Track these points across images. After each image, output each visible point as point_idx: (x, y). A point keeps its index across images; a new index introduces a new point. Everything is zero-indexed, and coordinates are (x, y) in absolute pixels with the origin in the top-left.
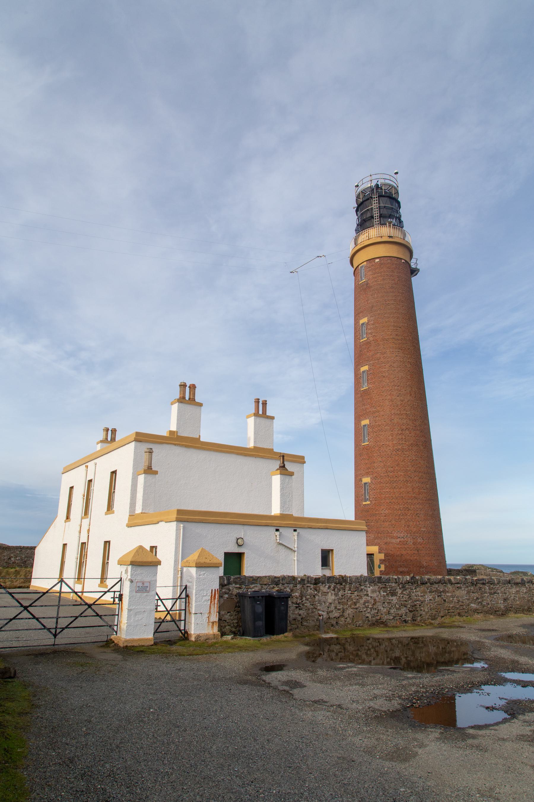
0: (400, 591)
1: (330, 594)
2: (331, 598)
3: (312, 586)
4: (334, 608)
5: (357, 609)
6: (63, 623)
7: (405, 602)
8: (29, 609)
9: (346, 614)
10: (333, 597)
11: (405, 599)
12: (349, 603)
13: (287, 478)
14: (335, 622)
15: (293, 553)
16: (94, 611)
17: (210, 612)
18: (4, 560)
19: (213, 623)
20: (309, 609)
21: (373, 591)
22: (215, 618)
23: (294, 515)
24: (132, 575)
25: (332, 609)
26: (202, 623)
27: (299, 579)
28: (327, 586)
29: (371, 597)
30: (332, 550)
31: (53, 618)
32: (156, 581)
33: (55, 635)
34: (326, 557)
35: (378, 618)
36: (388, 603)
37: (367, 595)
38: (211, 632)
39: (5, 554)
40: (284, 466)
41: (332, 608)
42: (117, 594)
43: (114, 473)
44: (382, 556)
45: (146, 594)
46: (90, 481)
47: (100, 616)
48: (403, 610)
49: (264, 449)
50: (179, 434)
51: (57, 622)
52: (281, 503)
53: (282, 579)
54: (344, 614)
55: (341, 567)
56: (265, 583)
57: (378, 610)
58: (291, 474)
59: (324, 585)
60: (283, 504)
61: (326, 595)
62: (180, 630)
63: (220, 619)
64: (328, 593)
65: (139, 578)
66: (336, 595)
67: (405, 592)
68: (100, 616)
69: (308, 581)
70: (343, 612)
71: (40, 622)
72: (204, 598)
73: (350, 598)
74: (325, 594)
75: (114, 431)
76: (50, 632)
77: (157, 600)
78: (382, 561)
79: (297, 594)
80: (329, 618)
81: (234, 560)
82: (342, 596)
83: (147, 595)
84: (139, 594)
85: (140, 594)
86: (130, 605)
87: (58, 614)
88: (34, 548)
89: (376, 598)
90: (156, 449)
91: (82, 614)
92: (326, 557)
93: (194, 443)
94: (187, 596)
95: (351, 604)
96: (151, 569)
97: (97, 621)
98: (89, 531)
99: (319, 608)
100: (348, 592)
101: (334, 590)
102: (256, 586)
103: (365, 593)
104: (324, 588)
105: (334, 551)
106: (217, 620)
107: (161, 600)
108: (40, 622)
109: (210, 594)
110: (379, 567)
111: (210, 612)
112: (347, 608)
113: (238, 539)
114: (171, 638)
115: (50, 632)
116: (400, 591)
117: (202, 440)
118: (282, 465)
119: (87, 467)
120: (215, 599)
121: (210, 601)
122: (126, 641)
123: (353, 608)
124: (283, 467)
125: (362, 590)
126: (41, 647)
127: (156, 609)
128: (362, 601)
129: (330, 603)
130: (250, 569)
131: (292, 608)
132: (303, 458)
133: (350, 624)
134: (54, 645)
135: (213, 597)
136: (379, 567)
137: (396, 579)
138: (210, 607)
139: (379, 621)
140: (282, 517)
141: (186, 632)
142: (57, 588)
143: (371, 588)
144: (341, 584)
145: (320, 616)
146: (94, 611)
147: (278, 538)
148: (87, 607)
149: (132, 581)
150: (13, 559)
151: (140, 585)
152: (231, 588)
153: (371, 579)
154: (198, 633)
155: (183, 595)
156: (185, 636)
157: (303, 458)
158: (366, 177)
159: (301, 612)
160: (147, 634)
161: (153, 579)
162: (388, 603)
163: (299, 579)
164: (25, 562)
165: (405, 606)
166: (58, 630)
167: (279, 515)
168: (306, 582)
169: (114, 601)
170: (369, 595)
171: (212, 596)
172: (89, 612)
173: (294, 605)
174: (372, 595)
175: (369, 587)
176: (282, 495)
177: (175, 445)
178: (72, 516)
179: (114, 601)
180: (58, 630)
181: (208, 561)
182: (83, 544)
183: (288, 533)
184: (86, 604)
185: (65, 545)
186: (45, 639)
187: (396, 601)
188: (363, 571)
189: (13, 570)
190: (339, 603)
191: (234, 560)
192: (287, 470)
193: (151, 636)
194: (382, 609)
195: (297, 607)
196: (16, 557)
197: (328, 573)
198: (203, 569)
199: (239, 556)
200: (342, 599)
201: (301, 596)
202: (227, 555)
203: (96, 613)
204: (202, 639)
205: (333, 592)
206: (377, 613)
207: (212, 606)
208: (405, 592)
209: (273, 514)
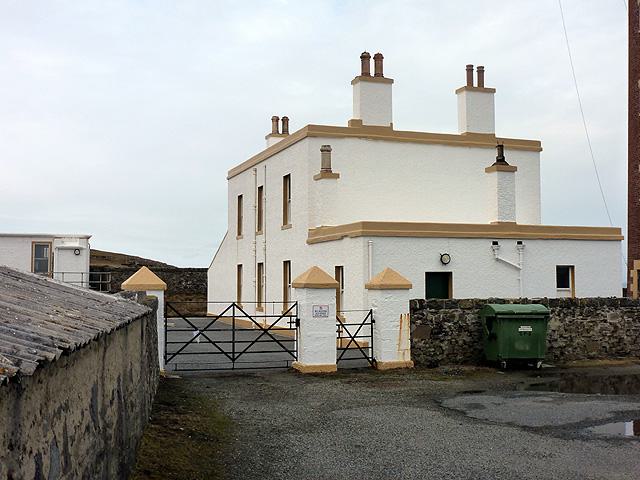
6: (239, 347)
13: (508, 175)
22: (407, 345)
26: (393, 348)
33: (233, 360)
34: (564, 275)
37: (605, 321)
42: (294, 319)
43: (287, 178)
46: (261, 188)
55: (585, 288)
58: (513, 170)
62: (368, 358)
63: (412, 347)
66: (561, 321)
75: (285, 120)
81: (438, 283)
89: (619, 325)
90: (333, 144)
92: (564, 275)
93: (385, 134)
97: (275, 346)
101: (559, 315)
107: (343, 326)
114: (356, 365)
124: (501, 160)
128: (597, 329)
129: (554, 331)
130: (459, 292)
134: (233, 369)
140: (501, 226)
141: (374, 360)
142: (229, 313)
153: (623, 302)
155: (369, 321)
166: (236, 355)
177: (360, 137)
182: (260, 265)
184: (262, 329)
185: (240, 266)
186: (224, 363)
188: (620, 295)
191: (438, 283)
197: (564, 294)
198: (389, 291)
199: (447, 276)
202: (431, 277)
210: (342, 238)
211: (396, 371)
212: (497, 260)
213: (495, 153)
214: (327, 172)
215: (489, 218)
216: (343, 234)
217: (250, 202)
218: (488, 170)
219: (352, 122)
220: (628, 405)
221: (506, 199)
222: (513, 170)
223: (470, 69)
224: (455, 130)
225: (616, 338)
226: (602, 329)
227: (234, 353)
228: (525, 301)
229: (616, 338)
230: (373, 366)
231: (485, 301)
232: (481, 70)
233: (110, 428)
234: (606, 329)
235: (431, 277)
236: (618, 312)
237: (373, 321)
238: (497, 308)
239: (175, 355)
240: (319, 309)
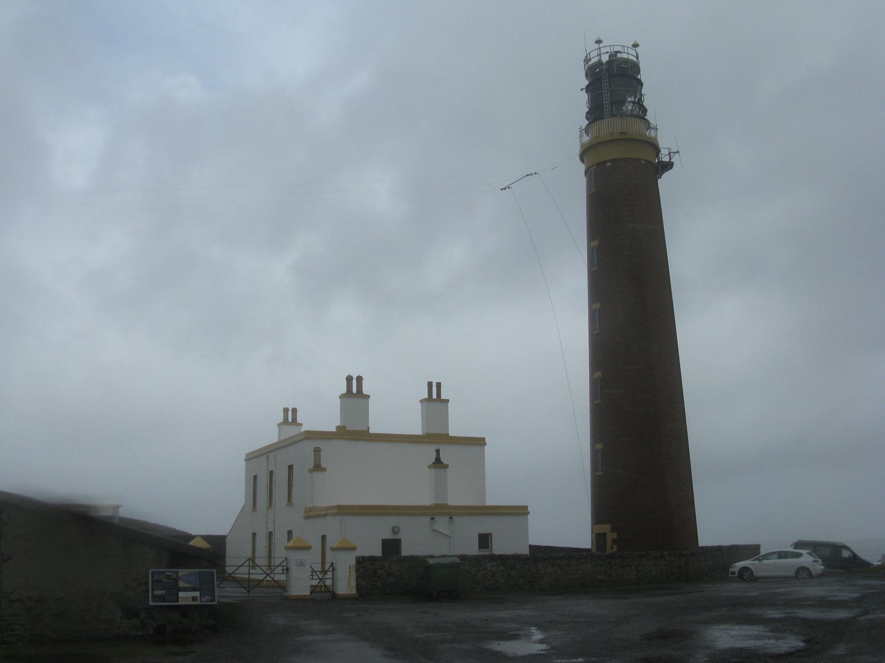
33: (249, 592)
44: (614, 536)
55: (499, 548)
58: (446, 466)
78: (614, 541)
81: (484, 540)
92: (484, 540)
93: (363, 436)
94: (333, 569)
110: (612, 548)
114: (323, 599)
117: (371, 431)
119: (268, 457)
126: (225, 600)
132: (526, 508)
136: (612, 548)
157: (526, 508)
158: (617, 39)
166: (247, 563)
178: (294, 500)
191: (391, 546)
197: (486, 552)
199: (398, 542)
202: (385, 543)
210: (326, 515)
211: (347, 598)
212: (434, 530)
214: (318, 467)
215: (426, 499)
217: (263, 482)
219: (338, 427)
222: (446, 466)
223: (430, 385)
224: (417, 430)
228: (445, 556)
230: (334, 596)
231: (425, 557)
232: (439, 385)
233: (205, 586)
235: (385, 543)
237: (333, 569)
238: (431, 561)
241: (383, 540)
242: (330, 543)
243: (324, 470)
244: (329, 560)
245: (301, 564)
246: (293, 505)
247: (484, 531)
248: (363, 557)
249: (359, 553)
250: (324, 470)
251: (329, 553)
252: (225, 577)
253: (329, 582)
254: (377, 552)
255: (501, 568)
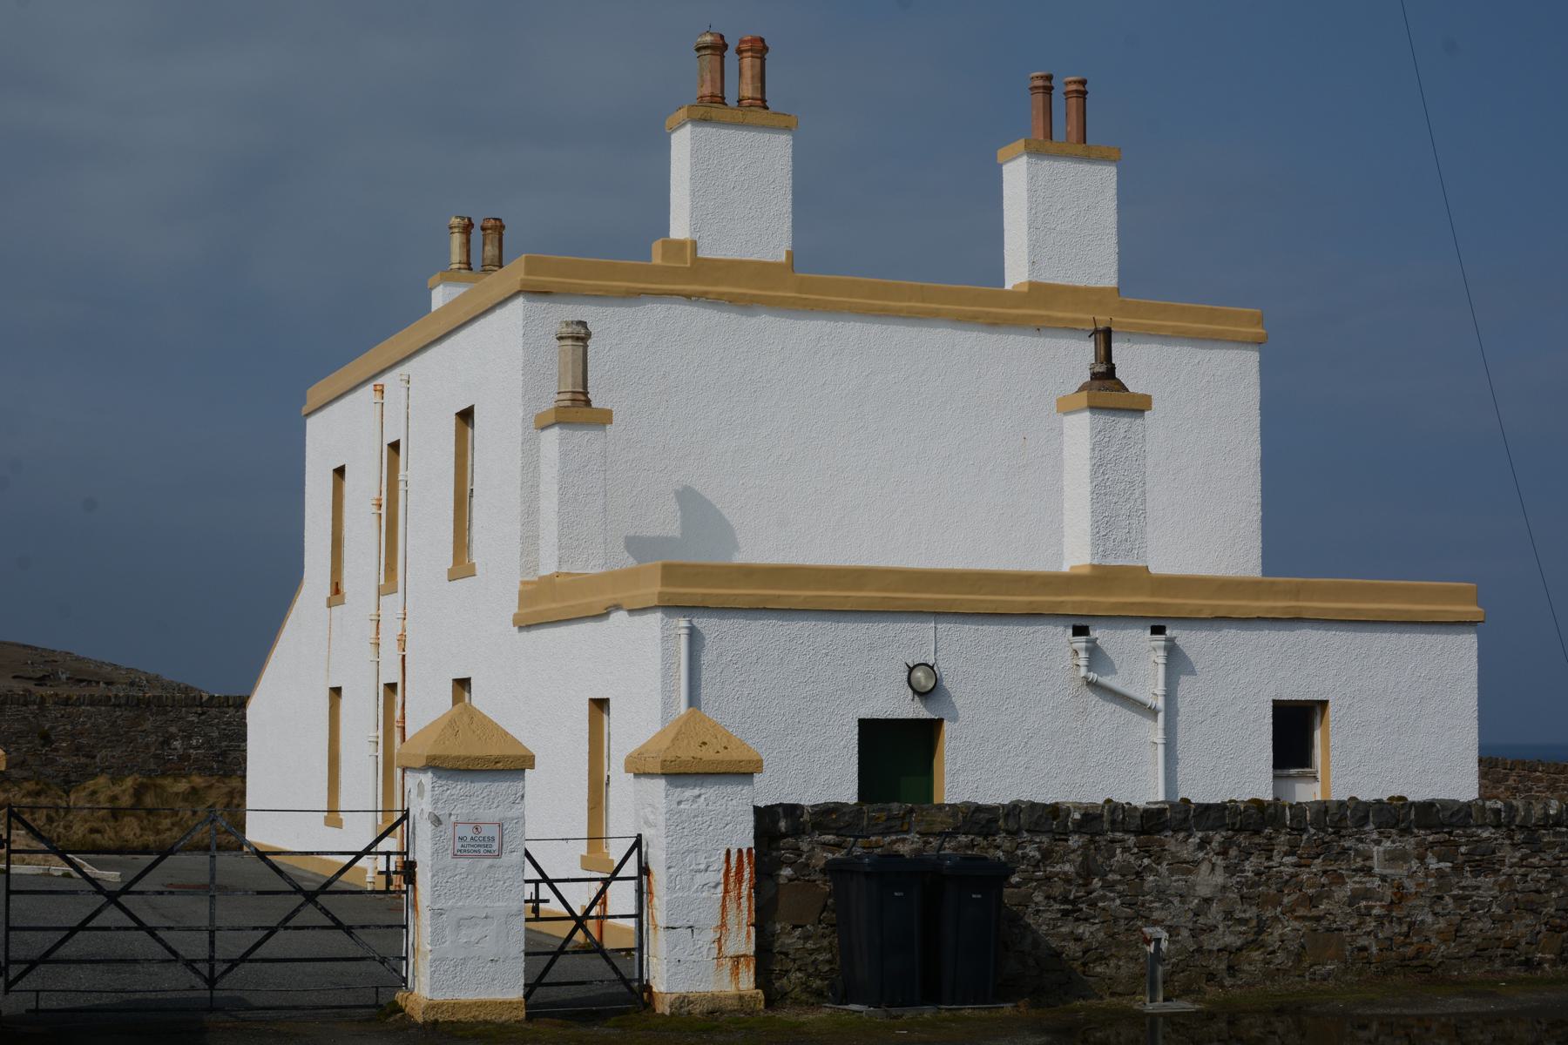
0: (1511, 856)
1: (1205, 867)
2: (1208, 880)
3: (1131, 840)
4: (1220, 917)
5: (1318, 919)
6: (230, 945)
7: (1534, 896)
8: (122, 899)
9: (1273, 937)
10: (1219, 878)
11: (1531, 885)
12: (1286, 900)
14: (1223, 966)
15: (1149, 723)
16: (327, 913)
17: (723, 925)
18: (147, 746)
19: (736, 959)
20: (1116, 920)
21: (1394, 858)
22: (742, 941)
23: (1153, 570)
24: (435, 802)
25: (1211, 922)
27: (1077, 816)
28: (1194, 840)
29: (1383, 878)
30: (1324, 704)
31: (199, 929)
32: (520, 820)
33: (211, 982)
34: (1295, 729)
35: (1410, 951)
36: (1456, 898)
37: (1368, 871)
38: (730, 989)
39: (148, 726)
40: (1110, 373)
41: (1215, 913)
45: (488, 862)
46: (395, 446)
47: (349, 930)
48: (1522, 926)
49: (1075, 290)
50: (703, 253)
51: (212, 943)
52: (1095, 524)
53: (1007, 816)
54: (1264, 936)
55: (1346, 771)
56: (937, 828)
57: (1411, 925)
58: (1138, 407)
59: (1181, 836)
60: (1103, 527)
61: (1189, 872)
64: (1197, 863)
65: (461, 811)
66: (1231, 870)
67: (1535, 860)
68: (349, 930)
69: (1113, 822)
70: (1260, 930)
71: (160, 941)
72: (700, 879)
73: (1292, 881)
74: (1187, 867)
76: (197, 972)
77: (537, 882)
79: (1067, 867)
80: (1199, 950)
82: (1258, 874)
83: (491, 866)
84: (464, 863)
85: (466, 862)
86: (436, 897)
87: (212, 917)
88: (241, 703)
89: (1407, 883)
91: (288, 919)
92: (1295, 729)
94: (644, 870)
95: (1297, 903)
96: (503, 787)
98: (402, 640)
99: (1156, 915)
100: (1285, 864)
101: (1224, 853)
102: (904, 840)
103: (1359, 862)
104: (1182, 846)
105: (1331, 708)
106: (751, 949)
107: (550, 883)
108: (160, 941)
109: (719, 863)
111: (723, 925)
112: (1276, 919)
113: (911, 670)
115: (197, 972)
116: (1511, 856)
118: (1101, 369)
120: (739, 881)
121: (721, 887)
122: (433, 1006)
123: (1303, 918)
124: (1105, 375)
125: (1345, 851)
127: (536, 910)
129: (1207, 901)
130: (968, 775)
131: (1048, 915)
133: (1286, 972)
135: (731, 876)
137: (1497, 812)
138: (724, 906)
139: (1415, 963)
140: (1102, 577)
143: (1387, 844)
144: (1257, 832)
145: (1148, 942)
146: (327, 913)
147: (1083, 662)
148: (300, 899)
149: (437, 821)
150: (177, 744)
151: (468, 832)
152: (804, 846)
154: (681, 988)
155: (631, 869)
156: (641, 994)
159: (1083, 929)
160: (500, 985)
161: (509, 814)
162: (1456, 898)
163: (1077, 816)
164: (224, 753)
165: (1533, 911)
167: (1086, 571)
168: (1106, 826)
169: (389, 882)
170: (1377, 870)
171: (727, 871)
172: (310, 915)
173: (1057, 906)
174: (1385, 872)
175: (1378, 843)
176: (1099, 492)
177: (688, 297)
178: (478, 555)
179: (389, 882)
180: (220, 968)
181: (707, 754)
182: (391, 687)
183: (1137, 660)
184: (298, 890)
185: (336, 692)
187: (1495, 892)
189: (183, 786)
190: (1242, 897)
191: (897, 752)
192: (1123, 388)
193: (516, 994)
194: (1430, 919)
195: (1065, 913)
196: (190, 737)
200: (1255, 885)
201: (1087, 872)
202: (873, 734)
203: (333, 919)
204: (697, 1010)
205: (1219, 861)
206: (1407, 935)
207: (732, 906)
208: (1535, 860)
209: (1066, 568)
210: (603, 616)
213: (1083, 353)
214: (577, 408)
216: (607, 598)
218: (1066, 407)
220: (803, 1018)
221: (1115, 496)
222: (1138, 407)
225: (1400, 921)
226: (1354, 898)
227: (211, 960)
229: (1400, 921)
234: (1367, 894)
235: (873, 734)
236: (1409, 843)
239: (32, 964)
240: (468, 832)
241: (861, 721)
242: (632, 730)
243: (603, 419)
244: (621, 826)
245: (481, 844)
246: (470, 572)
247: (1297, 691)
248: (792, 810)
249: (770, 790)
250: (603, 419)
251: (622, 787)
252: (239, 845)
253: (619, 932)
254: (834, 779)
255: (1433, 864)
